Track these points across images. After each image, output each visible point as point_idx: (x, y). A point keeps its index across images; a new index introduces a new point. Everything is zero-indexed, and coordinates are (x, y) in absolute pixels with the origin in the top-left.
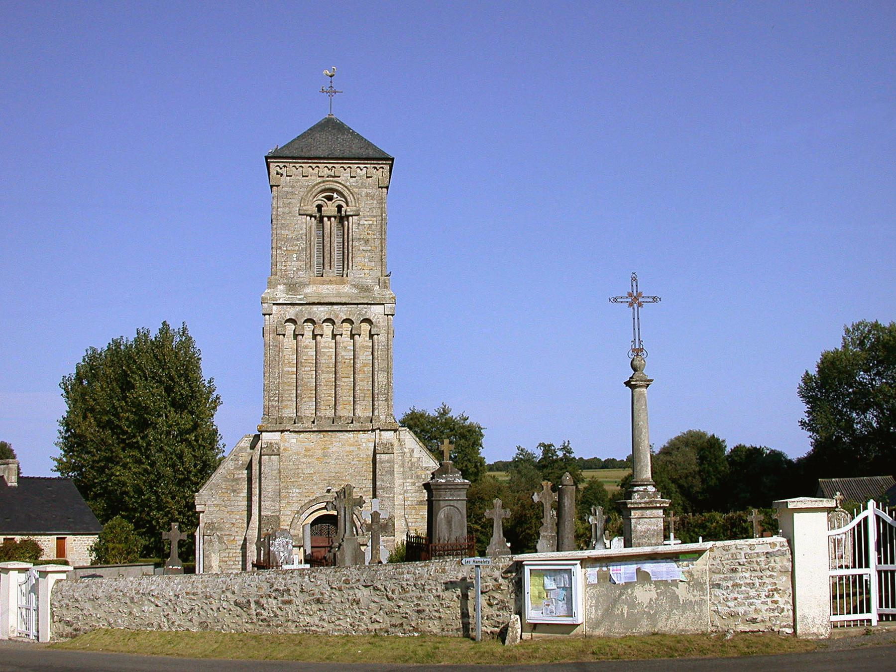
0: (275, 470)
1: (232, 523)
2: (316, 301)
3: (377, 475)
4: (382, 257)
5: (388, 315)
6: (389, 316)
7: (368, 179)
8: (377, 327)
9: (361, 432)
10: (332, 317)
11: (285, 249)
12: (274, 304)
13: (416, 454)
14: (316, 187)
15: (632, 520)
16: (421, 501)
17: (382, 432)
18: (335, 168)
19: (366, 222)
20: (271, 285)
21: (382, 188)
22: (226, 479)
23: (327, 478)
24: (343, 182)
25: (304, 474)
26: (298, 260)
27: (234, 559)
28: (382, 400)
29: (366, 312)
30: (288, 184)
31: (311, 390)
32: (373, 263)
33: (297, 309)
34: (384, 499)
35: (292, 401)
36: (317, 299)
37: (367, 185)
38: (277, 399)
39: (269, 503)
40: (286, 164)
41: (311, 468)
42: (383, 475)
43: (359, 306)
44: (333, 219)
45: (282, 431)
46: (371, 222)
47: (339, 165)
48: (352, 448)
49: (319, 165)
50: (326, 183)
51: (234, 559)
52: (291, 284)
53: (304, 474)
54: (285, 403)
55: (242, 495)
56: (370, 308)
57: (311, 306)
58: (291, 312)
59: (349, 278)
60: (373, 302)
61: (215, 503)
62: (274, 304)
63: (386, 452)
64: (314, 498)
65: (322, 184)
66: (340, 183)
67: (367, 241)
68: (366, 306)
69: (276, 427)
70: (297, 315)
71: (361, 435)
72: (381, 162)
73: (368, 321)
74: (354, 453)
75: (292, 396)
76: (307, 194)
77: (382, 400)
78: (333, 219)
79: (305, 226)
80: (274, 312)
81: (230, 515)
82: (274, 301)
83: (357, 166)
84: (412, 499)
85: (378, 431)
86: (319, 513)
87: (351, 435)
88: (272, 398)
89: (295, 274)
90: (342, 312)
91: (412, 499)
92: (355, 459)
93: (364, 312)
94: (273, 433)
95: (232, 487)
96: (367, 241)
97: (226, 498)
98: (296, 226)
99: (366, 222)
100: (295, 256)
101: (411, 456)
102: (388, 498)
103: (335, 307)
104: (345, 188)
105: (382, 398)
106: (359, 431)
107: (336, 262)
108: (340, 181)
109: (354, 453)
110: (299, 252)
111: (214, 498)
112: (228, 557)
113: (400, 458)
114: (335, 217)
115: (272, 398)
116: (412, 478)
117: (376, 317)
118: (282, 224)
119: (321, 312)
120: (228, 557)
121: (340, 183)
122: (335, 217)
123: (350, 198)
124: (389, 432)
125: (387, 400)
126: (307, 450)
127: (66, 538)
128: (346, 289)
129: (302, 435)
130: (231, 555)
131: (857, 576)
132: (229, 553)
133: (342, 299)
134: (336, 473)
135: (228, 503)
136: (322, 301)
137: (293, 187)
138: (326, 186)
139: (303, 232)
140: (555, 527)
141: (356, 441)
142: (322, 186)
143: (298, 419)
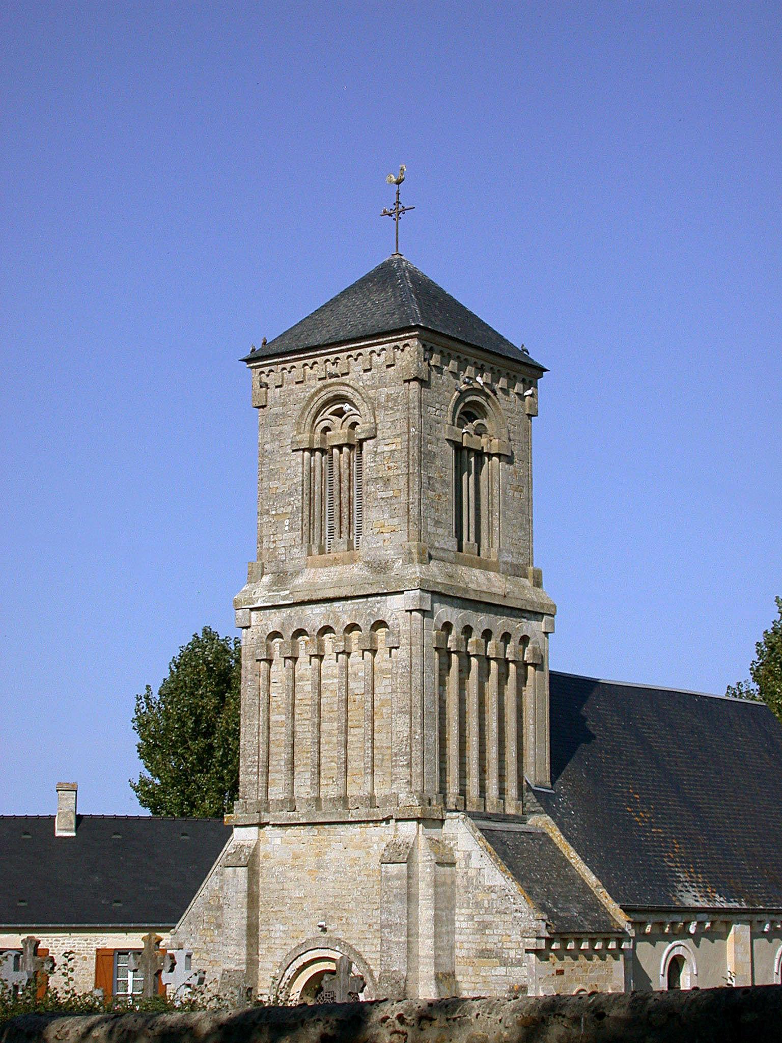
2: (306, 598)
5: (411, 611)
6: (413, 613)
7: (389, 369)
9: (371, 825)
11: (274, 512)
12: (252, 609)
13: (475, 863)
14: (316, 398)
15: (756, 984)
16: (483, 950)
17: (400, 823)
19: (386, 448)
20: (253, 577)
23: (322, 906)
25: (291, 898)
26: (291, 529)
28: (403, 766)
29: (379, 609)
30: (278, 400)
32: (396, 519)
36: (308, 595)
38: (255, 770)
39: (233, 948)
40: (272, 368)
42: (389, 902)
43: (369, 599)
44: (345, 449)
45: (261, 825)
46: (393, 447)
47: (342, 354)
49: (317, 359)
52: (281, 572)
53: (291, 898)
56: (385, 601)
57: (303, 607)
58: (274, 621)
59: (361, 552)
60: (385, 591)
61: (195, 945)
62: (252, 609)
63: (393, 859)
64: (303, 941)
66: (348, 385)
68: (379, 598)
69: (249, 818)
70: (283, 624)
71: (371, 829)
72: (402, 336)
73: (381, 624)
74: (361, 862)
76: (303, 413)
79: (300, 470)
80: (253, 623)
81: (213, 966)
82: (250, 604)
83: (370, 349)
84: (469, 945)
85: (392, 822)
86: (316, 968)
87: (356, 829)
88: (250, 770)
90: (345, 613)
91: (469, 945)
93: (376, 610)
94: (249, 828)
95: (216, 919)
97: (208, 939)
98: (289, 471)
100: (287, 522)
101: (467, 866)
103: (336, 604)
106: (368, 822)
108: (347, 382)
109: (361, 862)
111: (194, 938)
113: (428, 870)
116: (468, 908)
117: (394, 616)
119: (315, 616)
121: (348, 385)
124: (409, 823)
126: (296, 857)
128: (357, 571)
129: (290, 831)
131: (134, 979)
133: (342, 589)
136: (314, 598)
137: (284, 405)
142: (325, 396)
143: (291, 803)
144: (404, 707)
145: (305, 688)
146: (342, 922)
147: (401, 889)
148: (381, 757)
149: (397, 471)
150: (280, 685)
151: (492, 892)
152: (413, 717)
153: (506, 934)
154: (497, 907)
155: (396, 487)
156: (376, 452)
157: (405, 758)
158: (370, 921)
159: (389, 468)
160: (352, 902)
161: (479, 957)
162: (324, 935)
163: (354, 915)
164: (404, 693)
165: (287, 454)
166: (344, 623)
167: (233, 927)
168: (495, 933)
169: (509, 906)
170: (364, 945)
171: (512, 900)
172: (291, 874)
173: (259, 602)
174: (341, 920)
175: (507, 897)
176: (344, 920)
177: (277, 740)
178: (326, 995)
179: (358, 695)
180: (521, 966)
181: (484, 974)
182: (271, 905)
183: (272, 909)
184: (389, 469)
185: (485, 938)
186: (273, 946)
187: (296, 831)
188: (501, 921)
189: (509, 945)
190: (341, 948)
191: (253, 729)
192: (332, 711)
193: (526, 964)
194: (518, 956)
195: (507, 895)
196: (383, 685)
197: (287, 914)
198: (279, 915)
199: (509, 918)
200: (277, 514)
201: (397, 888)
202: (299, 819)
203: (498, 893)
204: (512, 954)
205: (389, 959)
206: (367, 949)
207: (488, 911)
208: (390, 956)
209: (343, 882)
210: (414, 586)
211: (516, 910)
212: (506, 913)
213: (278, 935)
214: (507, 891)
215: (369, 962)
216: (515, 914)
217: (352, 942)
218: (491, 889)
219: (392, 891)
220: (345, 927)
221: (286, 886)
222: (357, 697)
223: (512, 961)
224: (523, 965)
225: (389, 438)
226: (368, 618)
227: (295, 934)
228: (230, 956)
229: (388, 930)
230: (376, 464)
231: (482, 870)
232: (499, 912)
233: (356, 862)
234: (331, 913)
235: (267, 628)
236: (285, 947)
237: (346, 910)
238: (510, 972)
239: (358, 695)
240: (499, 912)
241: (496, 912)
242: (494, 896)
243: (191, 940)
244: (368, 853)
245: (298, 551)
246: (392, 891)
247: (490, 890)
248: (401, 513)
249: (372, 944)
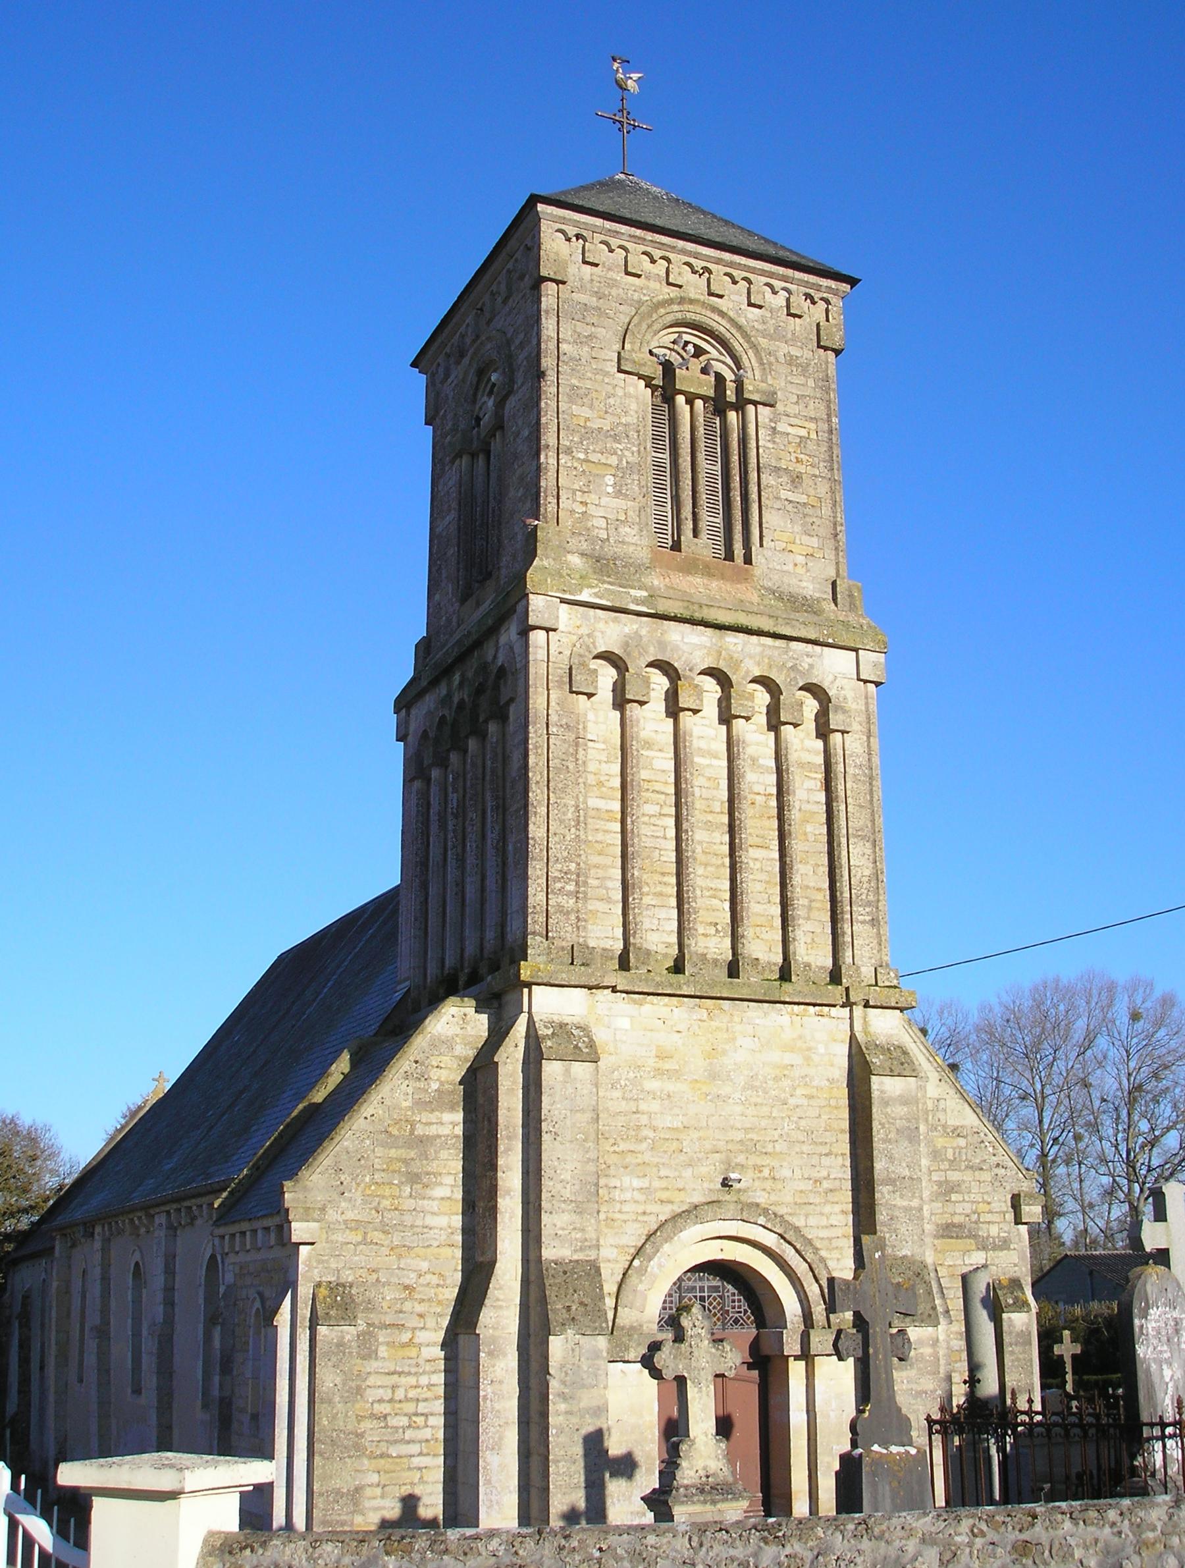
0: (583, 1111)
1: (406, 1287)
3: (875, 1139)
4: (835, 529)
5: (866, 682)
8: (845, 712)
10: (722, 665)
11: (582, 456)
12: (563, 601)
14: (662, 311)
18: (710, 272)
19: (790, 430)
21: (826, 349)
22: (387, 1138)
23: (721, 1145)
24: (731, 314)
26: (619, 494)
27: (410, 1407)
28: (863, 922)
30: (588, 285)
31: (663, 874)
33: (627, 630)
34: (897, 1213)
35: (609, 900)
37: (789, 336)
39: (566, 1217)
41: (676, 1111)
42: (890, 1141)
46: (803, 433)
48: (788, 1058)
50: (686, 307)
51: (410, 1407)
54: (593, 905)
55: (439, 1192)
61: (350, 1215)
62: (563, 601)
65: (676, 307)
67: (796, 480)
70: (627, 644)
75: (610, 884)
77: (863, 922)
78: (699, 403)
81: (400, 1257)
88: (558, 885)
89: (612, 532)
92: (798, 1092)
93: (807, 667)
96: (796, 480)
98: (612, 401)
99: (790, 430)
102: (907, 1209)
104: (733, 331)
105: (862, 913)
107: (711, 519)
110: (622, 472)
112: (391, 1401)
114: (705, 398)
115: (558, 885)
118: (573, 387)
120: (391, 1401)
122: (705, 398)
123: (749, 359)
125: (874, 922)
127: (36, 1509)
130: (400, 1394)
132: (394, 1388)
134: (747, 1130)
135: (392, 1218)
138: (689, 315)
139: (629, 419)
140: (644, 1237)
141: (800, 1037)
144: (862, 829)
145: (654, 762)
146: (761, 1175)
147: (909, 1120)
148: (806, 904)
149: (814, 466)
150: (603, 746)
151: (958, 1135)
152: (877, 848)
153: (984, 1202)
154: (966, 1160)
155: (812, 492)
156: (774, 429)
157: (868, 909)
158: (816, 1175)
159: (798, 461)
160: (780, 1141)
161: (943, 1237)
162: (728, 1197)
163: (785, 1164)
164: (861, 806)
165: (607, 374)
166: (747, 672)
167: (567, 1176)
168: (967, 1198)
169: (986, 1157)
170: (807, 1216)
171: (991, 1149)
172: (652, 1085)
173: (584, 593)
174: (760, 1171)
175: (982, 1145)
176: (766, 1172)
177: (597, 842)
178: (734, 1308)
179: (759, 794)
180: (1008, 1249)
181: (951, 1263)
182: (613, 1141)
183: (615, 1148)
184: (798, 462)
185: (950, 1208)
186: (617, 1216)
187: (665, 1009)
188: (974, 1180)
189: (989, 1217)
190: (768, 1221)
191: (564, 814)
192: (711, 812)
193: (1016, 1246)
194: (1002, 1235)
195: (983, 1142)
196: (805, 787)
197: (647, 1157)
198: (629, 1159)
199: (986, 1176)
200: (587, 461)
201: (901, 1119)
202: (680, 988)
203: (969, 1138)
204: (994, 1230)
205: (894, 1237)
206: (812, 1221)
207: (953, 1164)
208: (895, 1230)
209: (762, 1104)
210: (879, 647)
211: (998, 1165)
212: (981, 1169)
213: (628, 1196)
214: (982, 1135)
215: (818, 1244)
216: (997, 1171)
217: (781, 1210)
218: (957, 1132)
219: (893, 1124)
220: (768, 1184)
221: (643, 1106)
222: (758, 797)
223: (994, 1242)
224: (1012, 1247)
225: (795, 416)
226: (792, 675)
227: (665, 1195)
228: (560, 1232)
229: (890, 1188)
230: (775, 446)
231: (942, 1102)
232: (972, 1167)
233: (786, 1072)
234: (741, 1159)
235: (593, 643)
236: (645, 1218)
237: (770, 1154)
238: (993, 1259)
239: (759, 794)
240: (972, 1167)
241: (967, 1167)
242: (962, 1142)
243: (343, 1204)
244: (808, 1059)
245: (634, 532)
246: (893, 1124)
247: (956, 1134)
248: (822, 532)
249: (822, 1214)
